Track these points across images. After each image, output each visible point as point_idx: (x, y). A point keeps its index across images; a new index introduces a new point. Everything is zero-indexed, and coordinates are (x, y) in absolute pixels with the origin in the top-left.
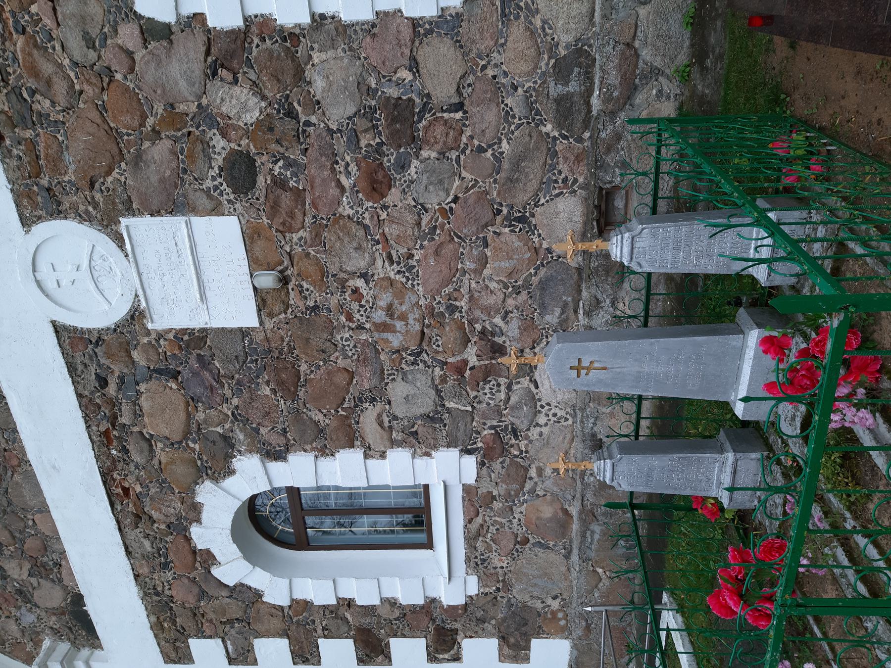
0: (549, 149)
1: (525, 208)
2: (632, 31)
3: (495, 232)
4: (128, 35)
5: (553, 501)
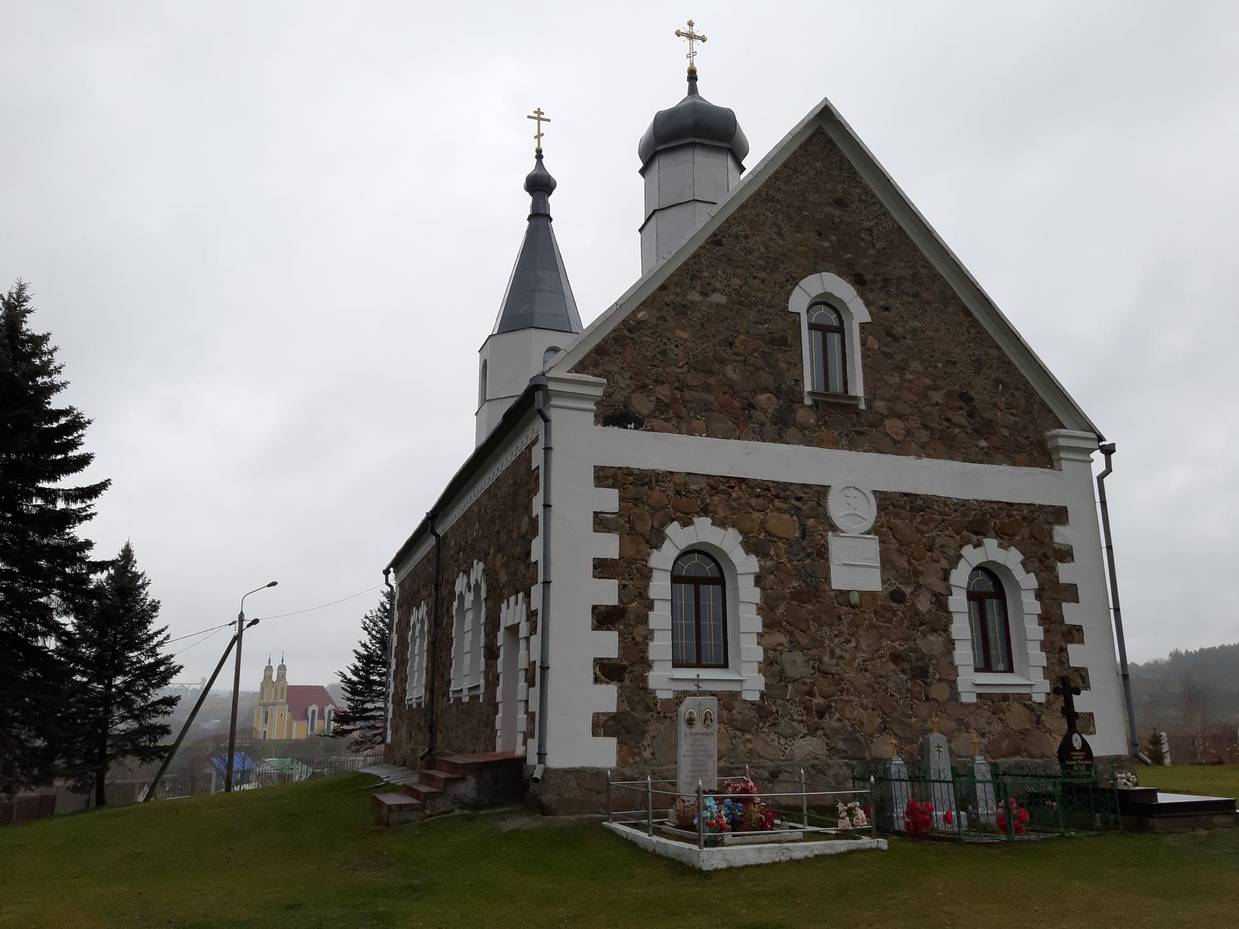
4: (944, 563)
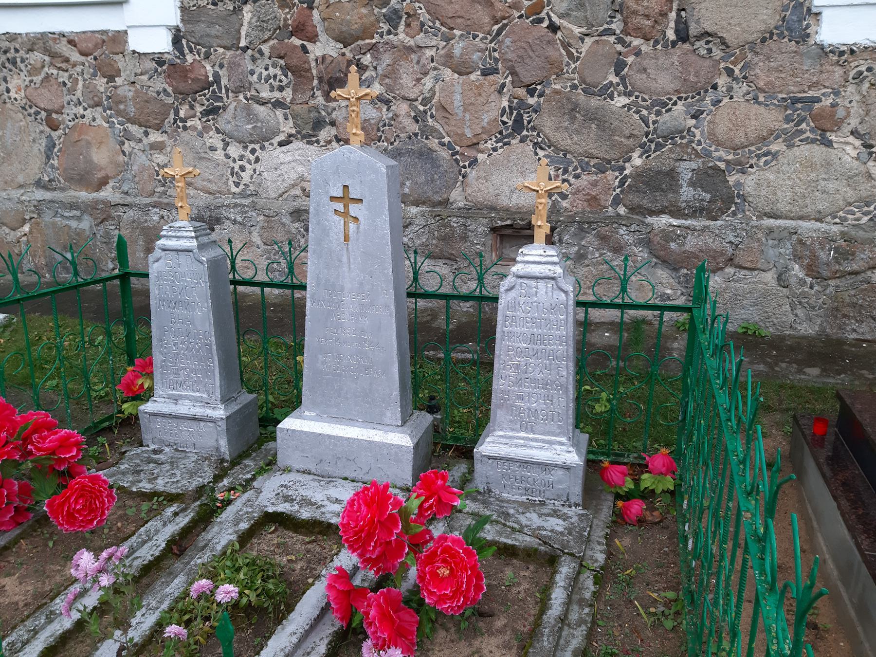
0: (609, 162)
1: (534, 129)
2: (748, 265)
3: (503, 86)
5: (118, 165)
